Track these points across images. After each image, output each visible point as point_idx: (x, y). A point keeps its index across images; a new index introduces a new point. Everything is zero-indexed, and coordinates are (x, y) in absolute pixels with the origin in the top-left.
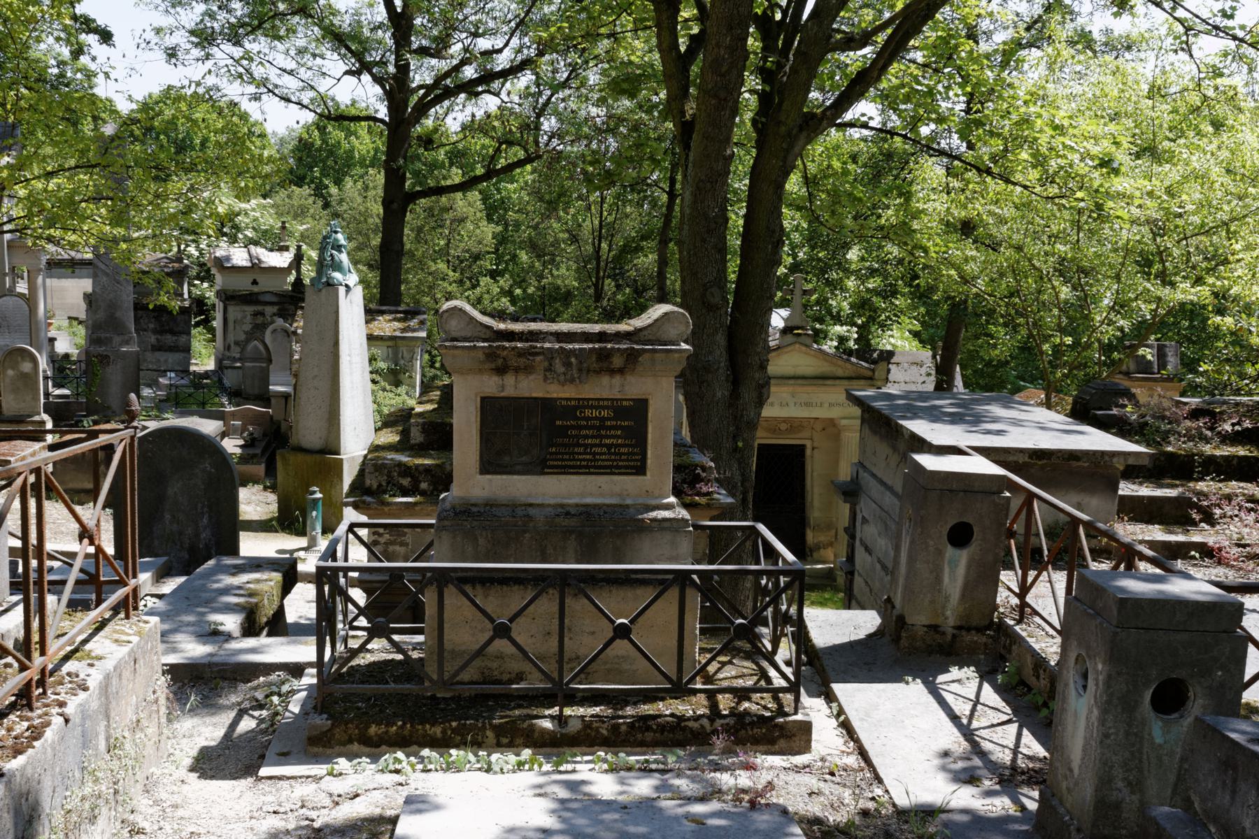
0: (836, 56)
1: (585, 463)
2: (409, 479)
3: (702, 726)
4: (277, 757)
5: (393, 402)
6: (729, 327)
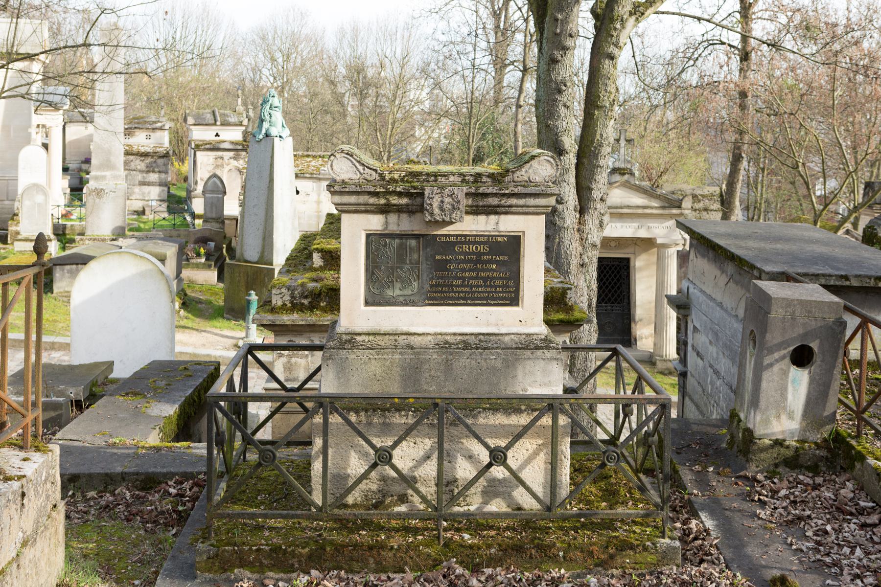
1: (462, 295)
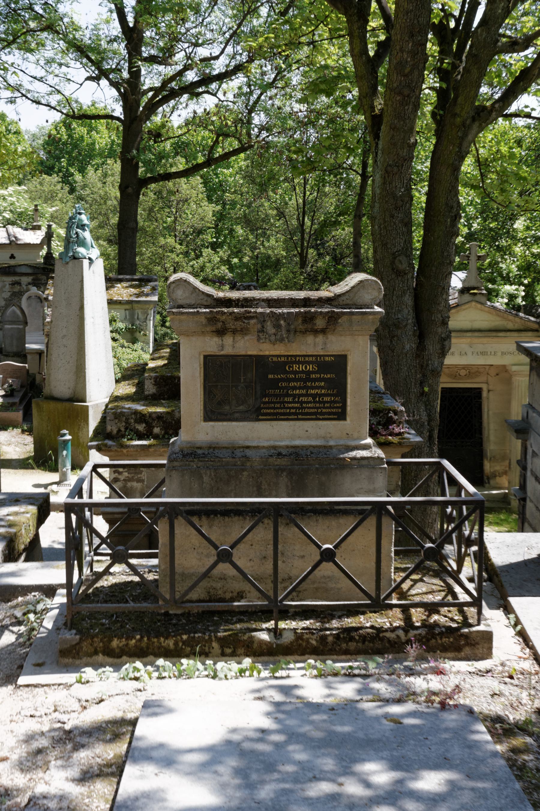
0: (502, 57)
1: (294, 411)
2: (144, 425)
3: (398, 636)
4: (33, 668)
5: (131, 356)
6: (415, 289)
